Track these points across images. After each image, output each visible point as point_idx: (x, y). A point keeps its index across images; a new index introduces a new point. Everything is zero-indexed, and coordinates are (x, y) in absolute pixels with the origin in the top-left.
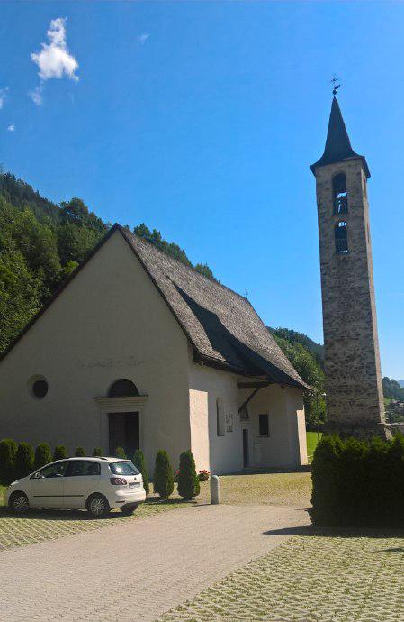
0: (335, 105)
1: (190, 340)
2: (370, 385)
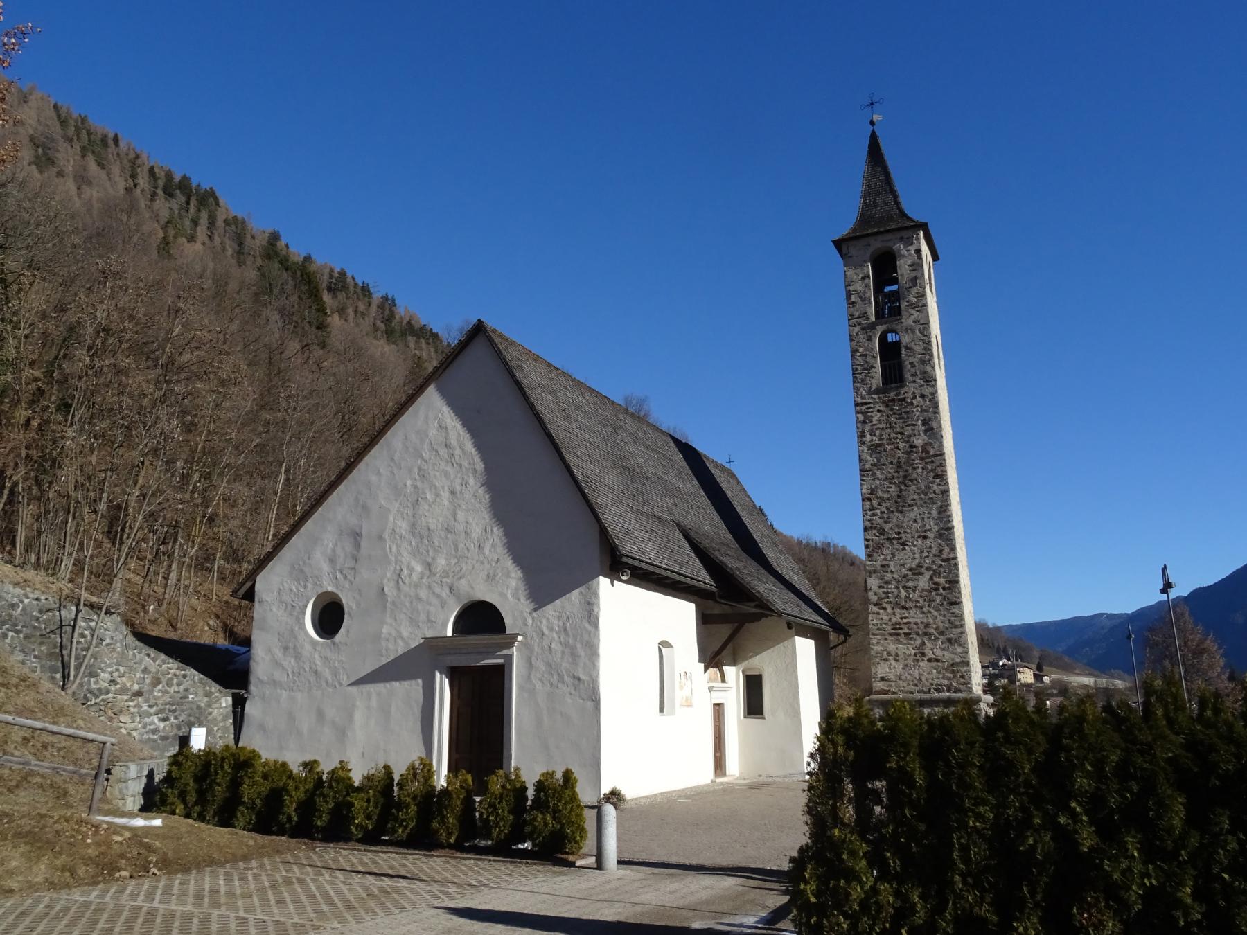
0: (873, 136)
1: (603, 532)
2: (950, 622)
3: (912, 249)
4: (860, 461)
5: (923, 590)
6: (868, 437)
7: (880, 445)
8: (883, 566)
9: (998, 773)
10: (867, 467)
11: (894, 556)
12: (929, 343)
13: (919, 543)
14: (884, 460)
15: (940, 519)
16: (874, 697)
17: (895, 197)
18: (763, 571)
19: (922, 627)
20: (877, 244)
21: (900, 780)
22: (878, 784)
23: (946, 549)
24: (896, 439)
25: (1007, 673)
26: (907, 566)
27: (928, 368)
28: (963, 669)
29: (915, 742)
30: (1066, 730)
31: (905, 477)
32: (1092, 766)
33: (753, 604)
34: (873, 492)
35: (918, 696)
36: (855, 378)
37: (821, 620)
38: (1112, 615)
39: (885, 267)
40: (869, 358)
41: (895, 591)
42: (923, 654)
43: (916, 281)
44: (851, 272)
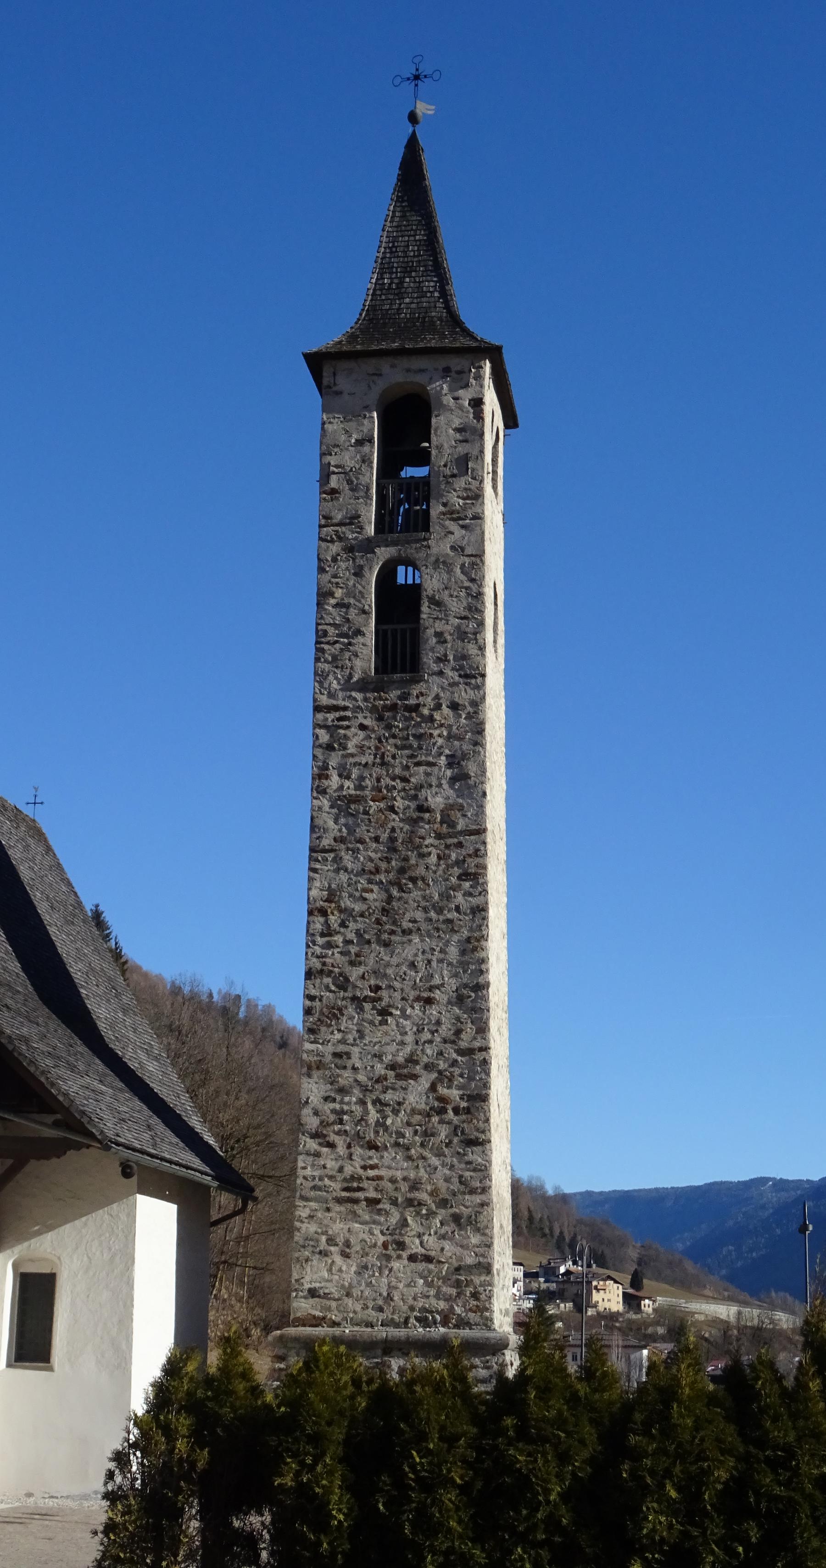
0: (413, 147)
2: (462, 1181)
3: (465, 395)
4: (313, 828)
5: (414, 1111)
6: (335, 780)
7: (356, 800)
8: (337, 1055)
9: (497, 1497)
10: (326, 842)
11: (361, 1034)
12: (479, 596)
13: (416, 1011)
14: (361, 831)
15: (464, 965)
16: (292, 1331)
17: (443, 280)
18: (81, 1048)
19: (404, 1187)
20: (395, 375)
21: (300, 1512)
22: (255, 1520)
23: (469, 1030)
24: (391, 789)
25: (573, 1289)
26: (388, 1058)
27: (472, 649)
28: (477, 1280)
29: (338, 1434)
30: (638, 1417)
31: (402, 871)
32: (679, 1490)
33: (50, 1119)
34: (332, 896)
35: (381, 1333)
36: (320, 650)
37: (196, 1162)
38: (782, 1181)
39: (406, 425)
40: (352, 613)
41: (358, 1110)
42: (401, 1245)
43: (466, 464)
44: (335, 426)
